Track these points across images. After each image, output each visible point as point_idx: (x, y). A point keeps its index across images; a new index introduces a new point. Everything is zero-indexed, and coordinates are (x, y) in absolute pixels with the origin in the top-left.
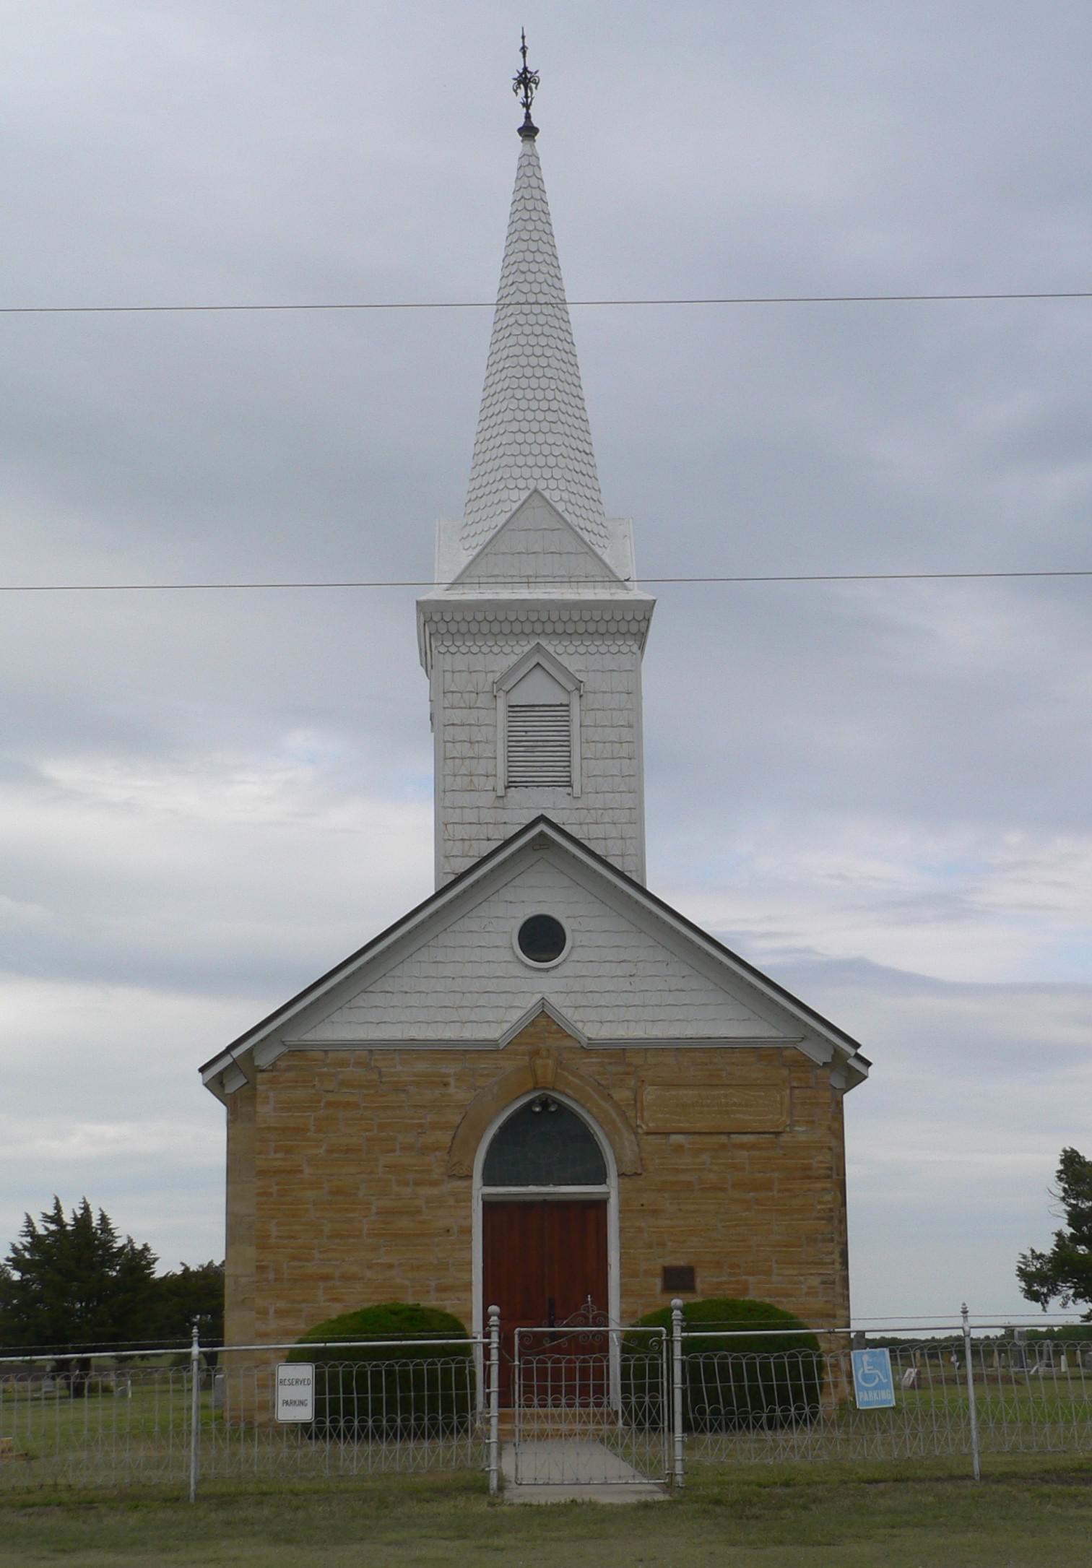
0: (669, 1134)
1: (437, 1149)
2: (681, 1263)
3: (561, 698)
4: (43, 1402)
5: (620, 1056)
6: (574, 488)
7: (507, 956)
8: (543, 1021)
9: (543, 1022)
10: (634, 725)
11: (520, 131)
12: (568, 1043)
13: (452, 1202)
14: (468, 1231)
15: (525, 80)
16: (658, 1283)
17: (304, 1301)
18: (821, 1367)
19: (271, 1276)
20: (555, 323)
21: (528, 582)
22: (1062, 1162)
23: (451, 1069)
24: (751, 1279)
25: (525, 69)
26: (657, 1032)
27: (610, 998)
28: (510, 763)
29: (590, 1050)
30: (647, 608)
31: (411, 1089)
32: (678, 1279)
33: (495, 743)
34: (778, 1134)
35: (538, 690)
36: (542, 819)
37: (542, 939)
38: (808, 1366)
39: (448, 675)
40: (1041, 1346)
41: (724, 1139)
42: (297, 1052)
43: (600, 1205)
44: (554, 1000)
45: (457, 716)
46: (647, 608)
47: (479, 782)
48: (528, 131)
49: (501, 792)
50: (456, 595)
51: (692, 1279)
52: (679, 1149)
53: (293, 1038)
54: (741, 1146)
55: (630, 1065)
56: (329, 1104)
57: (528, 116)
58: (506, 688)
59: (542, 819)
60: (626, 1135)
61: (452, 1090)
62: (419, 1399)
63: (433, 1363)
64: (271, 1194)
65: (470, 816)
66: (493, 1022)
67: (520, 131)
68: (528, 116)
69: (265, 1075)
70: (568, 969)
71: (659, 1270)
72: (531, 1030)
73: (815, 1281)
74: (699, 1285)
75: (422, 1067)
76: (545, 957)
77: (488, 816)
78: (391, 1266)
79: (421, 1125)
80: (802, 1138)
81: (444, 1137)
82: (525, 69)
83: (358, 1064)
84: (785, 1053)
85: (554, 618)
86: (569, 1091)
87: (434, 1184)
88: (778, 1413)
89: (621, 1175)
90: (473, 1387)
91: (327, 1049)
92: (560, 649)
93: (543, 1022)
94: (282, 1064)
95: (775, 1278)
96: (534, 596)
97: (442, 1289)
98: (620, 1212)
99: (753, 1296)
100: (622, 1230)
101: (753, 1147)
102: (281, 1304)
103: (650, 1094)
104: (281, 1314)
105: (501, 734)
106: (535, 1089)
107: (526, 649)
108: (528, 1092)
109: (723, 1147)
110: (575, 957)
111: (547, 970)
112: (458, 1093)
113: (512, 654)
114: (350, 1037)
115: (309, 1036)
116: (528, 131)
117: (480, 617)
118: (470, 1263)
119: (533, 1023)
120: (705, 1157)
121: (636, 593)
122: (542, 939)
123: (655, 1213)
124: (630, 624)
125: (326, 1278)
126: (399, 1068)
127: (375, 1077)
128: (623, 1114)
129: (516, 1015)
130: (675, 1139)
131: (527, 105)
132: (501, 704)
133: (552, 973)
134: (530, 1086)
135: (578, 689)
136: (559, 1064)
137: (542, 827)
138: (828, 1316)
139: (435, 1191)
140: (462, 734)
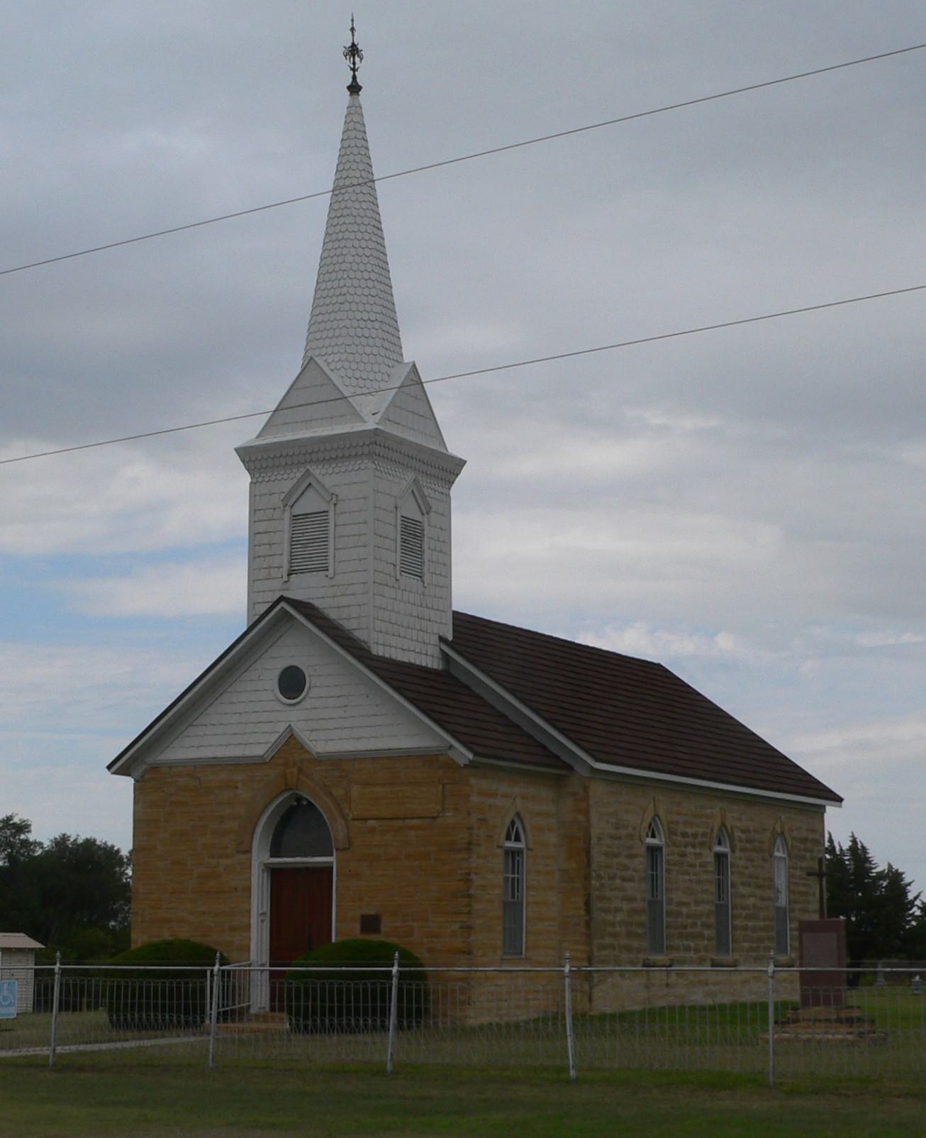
0: (365, 819)
2: (372, 912)
5: (338, 763)
9: (290, 742)
11: (349, 88)
15: (353, 51)
16: (358, 926)
18: (427, 993)
22: (87, 841)
25: (353, 45)
26: (362, 745)
29: (320, 760)
34: (434, 818)
35: (310, 503)
36: (282, 599)
37: (292, 683)
38: (418, 992)
40: (187, 983)
41: (400, 823)
42: (155, 768)
44: (299, 728)
47: (274, 572)
48: (354, 88)
49: (285, 578)
50: (257, 443)
52: (372, 830)
53: (151, 759)
57: (354, 77)
58: (290, 503)
66: (259, 746)
67: (349, 88)
68: (354, 77)
73: (456, 927)
74: (383, 928)
78: (204, 913)
82: (353, 45)
85: (316, 449)
88: (310, 1023)
91: (171, 765)
93: (290, 742)
94: (147, 777)
97: (233, 929)
103: (355, 791)
105: (286, 536)
107: (299, 475)
110: (311, 695)
116: (354, 88)
118: (249, 911)
122: (292, 683)
129: (273, 738)
130: (371, 823)
131: (354, 70)
132: (287, 516)
136: (300, 770)
137: (283, 604)
138: (464, 952)
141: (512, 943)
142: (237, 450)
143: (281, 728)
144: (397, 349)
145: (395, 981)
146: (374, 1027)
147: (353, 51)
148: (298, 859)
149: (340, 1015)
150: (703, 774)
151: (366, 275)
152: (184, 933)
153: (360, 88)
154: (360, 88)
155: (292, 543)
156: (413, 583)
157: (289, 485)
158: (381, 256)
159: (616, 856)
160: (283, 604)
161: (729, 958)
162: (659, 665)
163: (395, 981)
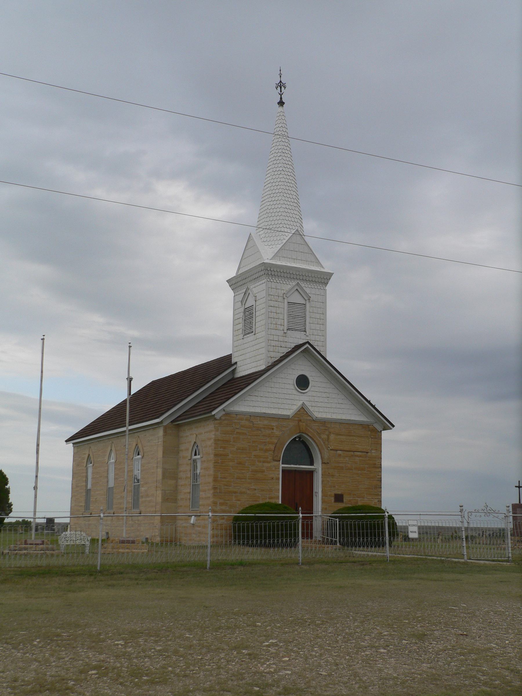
1: (270, 451)
2: (340, 493)
3: (303, 302)
5: (324, 422)
7: (292, 387)
8: (302, 410)
9: (303, 410)
10: (324, 314)
11: (278, 103)
12: (309, 418)
13: (274, 469)
14: (278, 479)
15: (281, 85)
16: (333, 499)
17: (228, 500)
19: (218, 491)
21: (295, 260)
23: (274, 424)
24: (359, 499)
25: (281, 81)
26: (334, 416)
27: (324, 404)
28: (289, 322)
30: (329, 275)
31: (262, 429)
32: (339, 498)
33: (284, 314)
35: (297, 298)
37: (303, 382)
39: (270, 289)
41: (352, 453)
43: (311, 473)
44: (307, 404)
45: (272, 303)
46: (329, 275)
48: (281, 103)
51: (343, 498)
52: (340, 455)
54: (357, 456)
55: (327, 427)
56: (237, 433)
57: (281, 98)
59: (308, 343)
60: (326, 450)
61: (275, 431)
62: (257, 535)
63: (307, 522)
64: (219, 463)
65: (276, 338)
67: (278, 103)
68: (281, 98)
69: (218, 421)
70: (310, 394)
71: (333, 495)
72: (299, 413)
75: (266, 422)
76: (303, 388)
77: (281, 339)
79: (264, 442)
80: (374, 454)
81: (272, 447)
82: (281, 81)
83: (246, 420)
84: (370, 427)
86: (309, 434)
87: (269, 462)
89: (323, 463)
90: (298, 530)
91: (237, 414)
93: (303, 410)
94: (223, 418)
95: (366, 499)
96: (282, 264)
97: (270, 498)
98: (322, 475)
99: (360, 504)
100: (323, 481)
101: (360, 456)
102: (221, 501)
103: (332, 437)
104: (221, 504)
105: (286, 311)
106: (300, 432)
108: (297, 434)
109: (352, 456)
111: (304, 393)
112: (277, 432)
113: (289, 285)
114: (248, 410)
115: (232, 409)
116: (281, 103)
117: (313, 276)
119: (299, 411)
120: (347, 459)
121: (327, 269)
122: (303, 382)
123: (333, 476)
124: (323, 279)
125: (235, 493)
126: (259, 422)
127: (252, 424)
128: (324, 443)
133: (305, 394)
134: (299, 431)
135: (309, 300)
137: (307, 345)
139: (269, 465)
140: (274, 310)
142: (331, 274)
143: (300, 403)
145: (300, 521)
146: (243, 544)
147: (281, 85)
148: (292, 466)
149: (265, 538)
150: (145, 419)
152: (360, 502)
153: (284, 103)
154: (284, 103)
155: (305, 317)
157: (289, 287)
160: (307, 345)
162: (153, 383)
163: (300, 521)
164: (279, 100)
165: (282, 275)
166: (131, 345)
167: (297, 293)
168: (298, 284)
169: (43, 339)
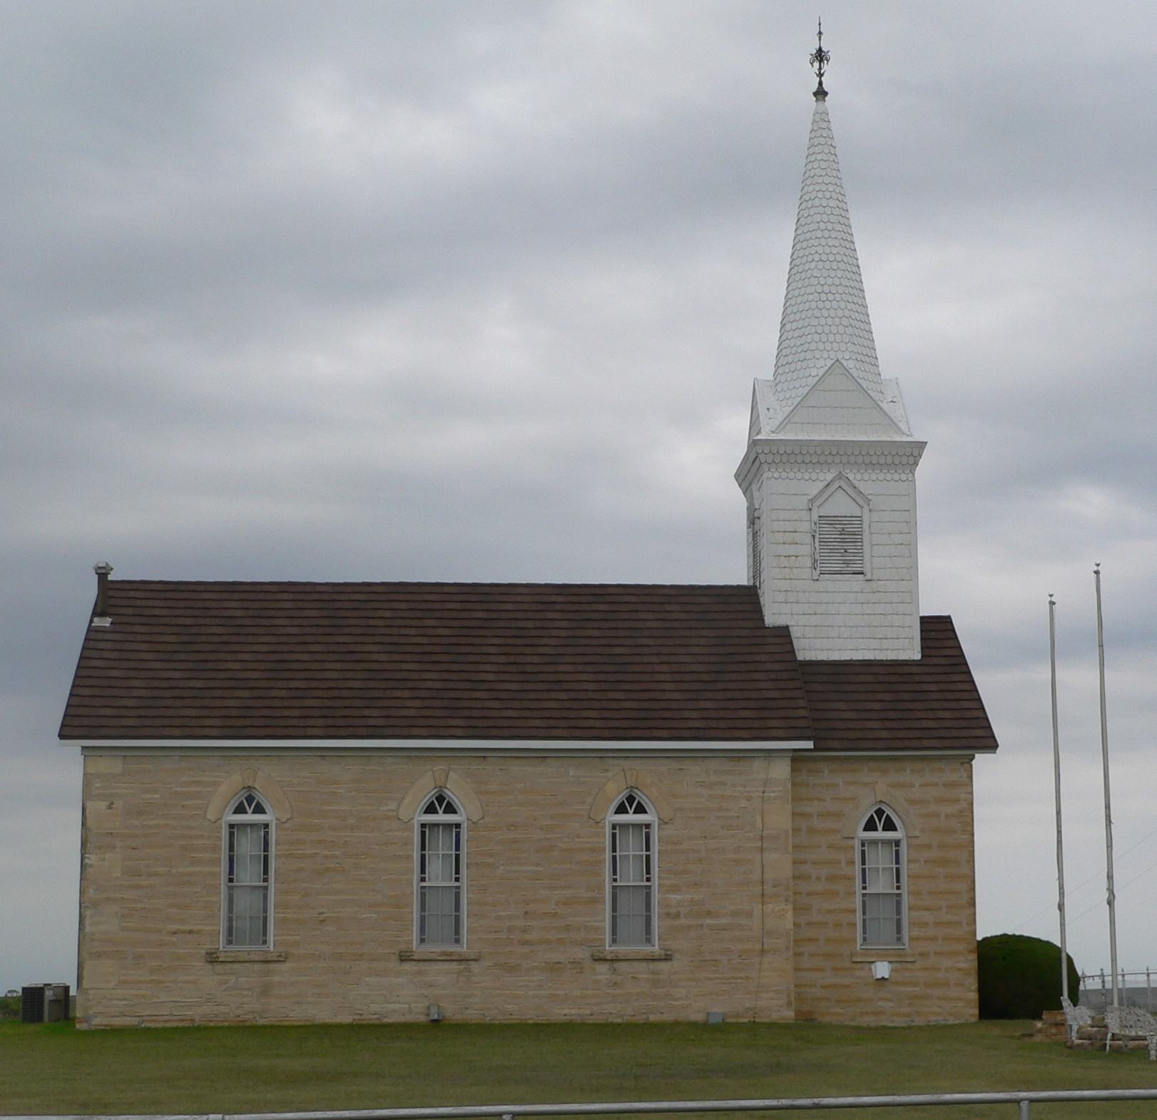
4: (895, 866)
6: (855, 340)
11: (815, 94)
15: (820, 56)
20: (839, 227)
25: (820, 50)
35: (840, 505)
48: (821, 93)
50: (774, 437)
57: (820, 83)
67: (815, 94)
68: (820, 83)
82: (820, 50)
92: (859, 476)
107: (830, 477)
113: (813, 482)
116: (821, 93)
124: (910, 454)
141: (1145, 1039)
144: (951, 643)
147: (820, 56)
151: (840, 313)
153: (826, 94)
154: (826, 94)
156: (856, 583)
158: (873, 361)
159: (678, 915)
161: (656, 949)
162: (1005, 935)
164: (825, 67)
165: (822, 459)
166: (1053, 599)
167: (840, 491)
168: (840, 476)
169: (1097, 573)
